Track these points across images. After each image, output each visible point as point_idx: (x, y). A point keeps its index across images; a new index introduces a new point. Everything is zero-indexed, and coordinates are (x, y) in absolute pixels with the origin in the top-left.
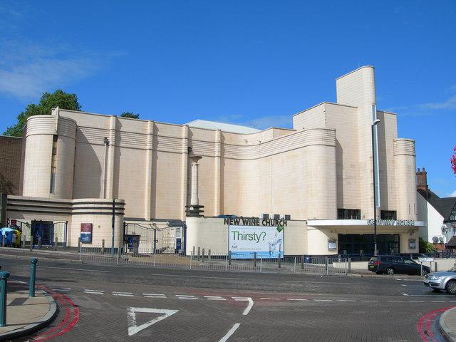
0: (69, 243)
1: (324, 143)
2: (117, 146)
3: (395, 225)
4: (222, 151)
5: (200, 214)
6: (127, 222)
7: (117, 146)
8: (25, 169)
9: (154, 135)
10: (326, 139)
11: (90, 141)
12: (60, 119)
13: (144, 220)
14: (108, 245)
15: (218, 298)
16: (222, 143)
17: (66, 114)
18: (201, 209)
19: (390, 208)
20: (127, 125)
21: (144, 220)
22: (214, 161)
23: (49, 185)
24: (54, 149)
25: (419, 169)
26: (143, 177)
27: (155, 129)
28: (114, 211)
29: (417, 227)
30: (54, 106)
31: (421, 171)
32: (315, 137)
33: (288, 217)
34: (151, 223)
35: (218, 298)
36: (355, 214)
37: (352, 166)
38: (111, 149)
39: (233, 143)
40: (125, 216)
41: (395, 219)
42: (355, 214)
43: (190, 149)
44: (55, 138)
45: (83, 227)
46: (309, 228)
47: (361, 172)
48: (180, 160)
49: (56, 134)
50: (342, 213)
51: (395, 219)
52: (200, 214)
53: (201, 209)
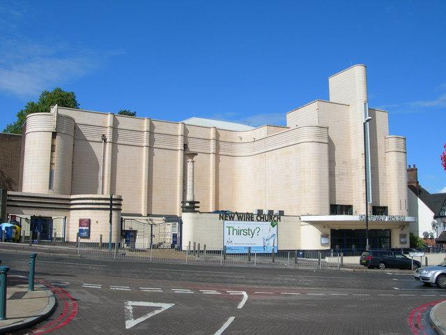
0: (68, 238)
1: (317, 140)
2: (114, 144)
3: (386, 220)
4: (217, 148)
5: (196, 209)
6: (124, 217)
7: (114, 143)
8: (25, 166)
9: (151, 132)
10: (319, 136)
11: (88, 138)
12: (59, 116)
13: (140, 215)
14: (106, 240)
15: (214, 292)
16: (217, 140)
17: (65, 112)
18: (196, 205)
19: (382, 204)
20: (125, 122)
21: (140, 215)
22: (209, 158)
23: (48, 181)
24: (53, 146)
25: (410, 166)
26: (140, 173)
27: (152, 126)
28: (111, 207)
29: (408, 222)
30: (53, 104)
31: (412, 167)
32: (308, 134)
33: (281, 213)
34: (148, 218)
35: (214, 292)
36: (347, 209)
37: (344, 162)
38: (109, 146)
39: (228, 140)
40: (122, 212)
41: (387, 215)
42: (347, 209)
43: (185, 146)
44: (54, 135)
45: (81, 222)
46: (302, 223)
47: (353, 169)
48: (176, 156)
49: (55, 131)
50: (335, 209)
51: (387, 215)
52: (196, 209)
53: (196, 205)
